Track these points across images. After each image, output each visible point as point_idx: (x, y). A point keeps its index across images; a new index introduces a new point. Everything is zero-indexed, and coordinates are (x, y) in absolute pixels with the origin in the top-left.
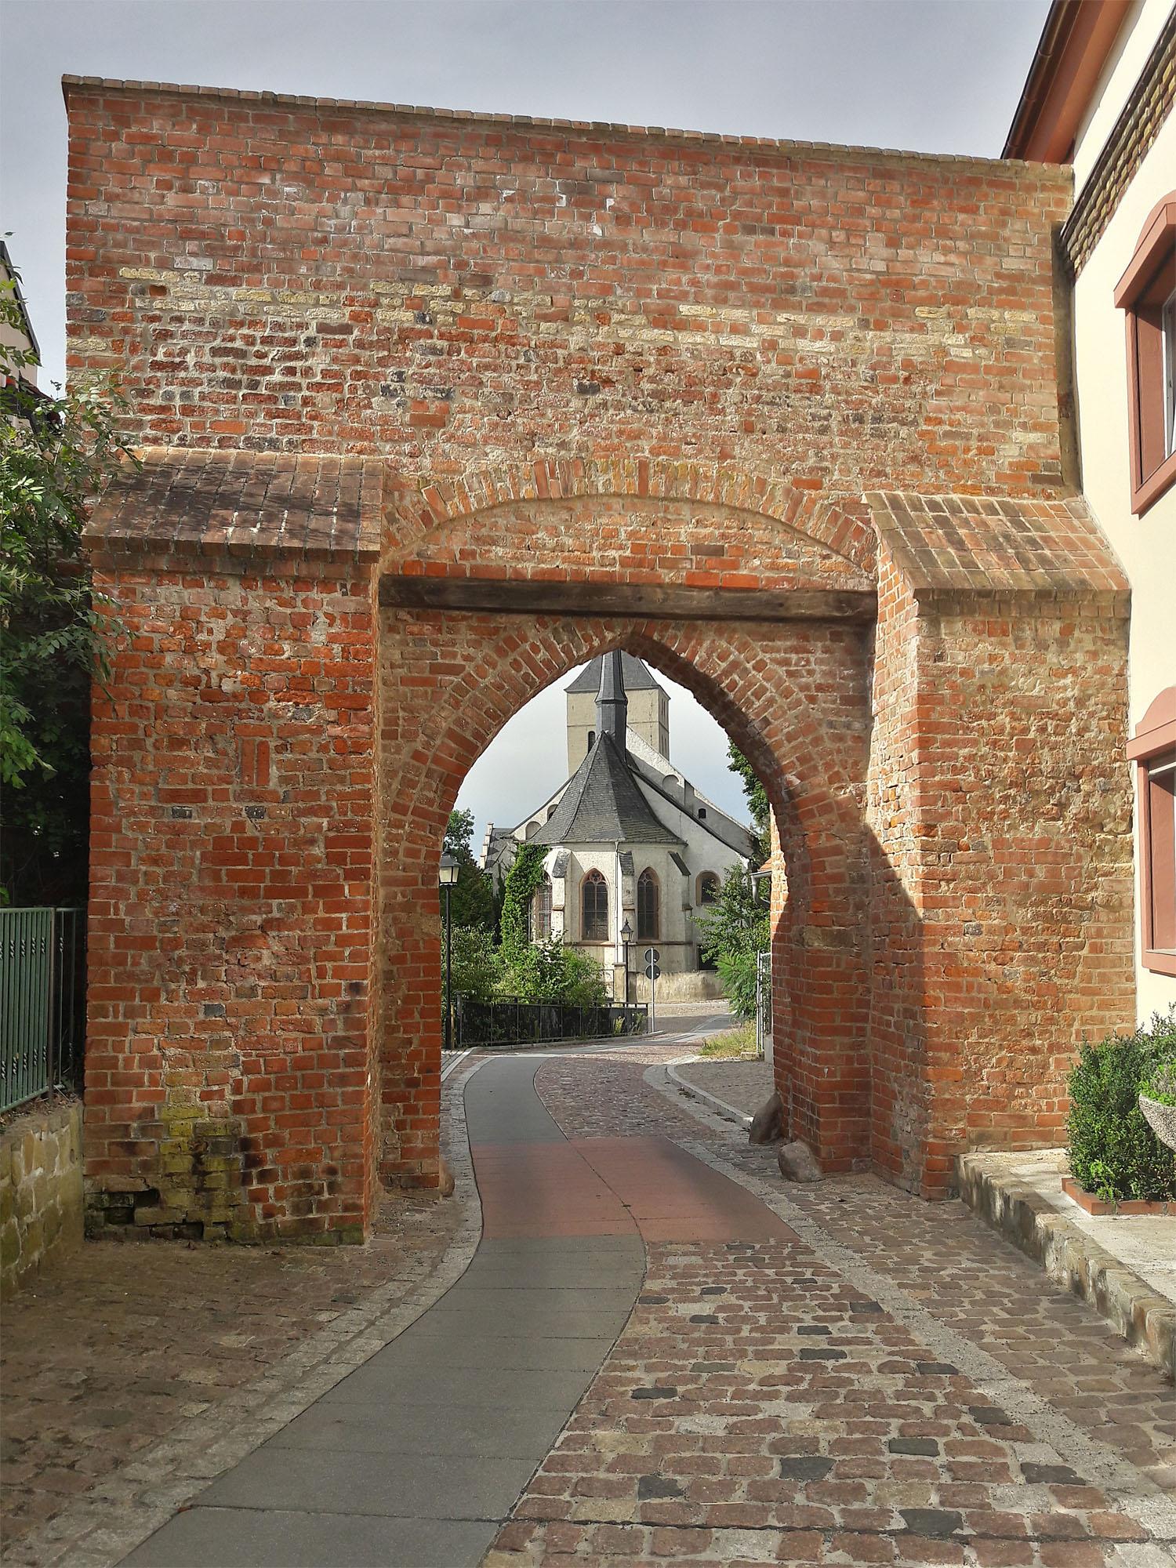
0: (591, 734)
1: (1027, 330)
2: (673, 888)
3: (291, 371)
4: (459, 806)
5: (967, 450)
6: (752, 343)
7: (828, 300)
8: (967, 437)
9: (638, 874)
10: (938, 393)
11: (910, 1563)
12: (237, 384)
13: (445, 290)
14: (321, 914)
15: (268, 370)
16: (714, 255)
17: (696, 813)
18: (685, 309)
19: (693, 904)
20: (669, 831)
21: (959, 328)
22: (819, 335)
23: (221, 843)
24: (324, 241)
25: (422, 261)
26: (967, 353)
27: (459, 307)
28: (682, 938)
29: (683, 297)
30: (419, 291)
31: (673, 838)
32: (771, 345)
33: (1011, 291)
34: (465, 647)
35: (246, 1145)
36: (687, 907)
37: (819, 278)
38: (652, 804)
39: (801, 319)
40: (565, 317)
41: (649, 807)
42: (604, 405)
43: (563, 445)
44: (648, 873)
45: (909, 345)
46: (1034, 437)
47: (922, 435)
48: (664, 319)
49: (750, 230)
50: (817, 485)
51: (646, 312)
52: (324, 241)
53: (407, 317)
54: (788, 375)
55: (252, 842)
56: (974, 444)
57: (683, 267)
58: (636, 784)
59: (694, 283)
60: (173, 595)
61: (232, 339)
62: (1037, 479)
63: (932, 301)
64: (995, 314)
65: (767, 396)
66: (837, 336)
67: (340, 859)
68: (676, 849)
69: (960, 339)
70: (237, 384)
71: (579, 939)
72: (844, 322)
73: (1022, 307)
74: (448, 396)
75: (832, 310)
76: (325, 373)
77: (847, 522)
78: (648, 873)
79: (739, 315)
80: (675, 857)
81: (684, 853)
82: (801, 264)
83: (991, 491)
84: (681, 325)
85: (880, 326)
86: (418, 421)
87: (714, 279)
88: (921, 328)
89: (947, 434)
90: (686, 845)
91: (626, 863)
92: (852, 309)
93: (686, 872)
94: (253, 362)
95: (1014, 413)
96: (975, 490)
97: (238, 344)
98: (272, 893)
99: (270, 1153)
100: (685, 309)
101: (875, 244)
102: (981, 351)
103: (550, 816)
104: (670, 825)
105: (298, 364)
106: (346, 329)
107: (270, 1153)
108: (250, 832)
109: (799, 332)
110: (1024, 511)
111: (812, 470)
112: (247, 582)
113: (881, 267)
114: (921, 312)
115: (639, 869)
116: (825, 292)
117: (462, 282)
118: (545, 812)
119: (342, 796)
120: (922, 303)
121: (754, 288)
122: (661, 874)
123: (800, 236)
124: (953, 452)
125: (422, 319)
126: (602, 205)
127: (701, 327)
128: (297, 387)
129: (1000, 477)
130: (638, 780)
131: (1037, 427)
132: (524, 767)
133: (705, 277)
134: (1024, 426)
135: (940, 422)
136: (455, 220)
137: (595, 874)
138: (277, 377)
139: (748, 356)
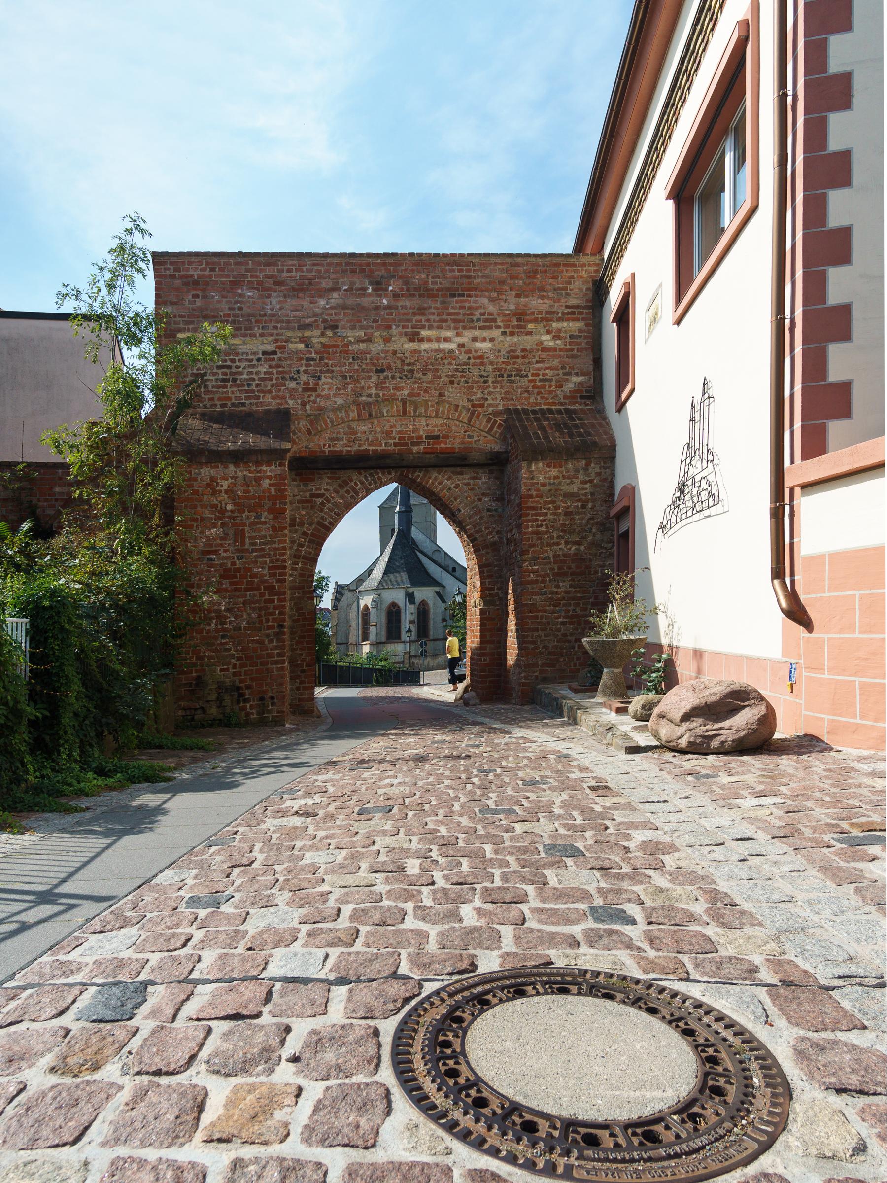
1: (580, 331)
3: (251, 373)
5: (550, 386)
6: (453, 346)
7: (489, 322)
8: (551, 380)
10: (537, 362)
12: (227, 380)
13: (317, 333)
14: (267, 597)
15: (241, 373)
16: (436, 308)
18: (424, 333)
21: (548, 332)
22: (484, 340)
23: (226, 570)
24: (265, 315)
25: (308, 321)
26: (551, 343)
27: (323, 340)
29: (423, 327)
30: (307, 333)
32: (461, 346)
33: (573, 313)
34: (324, 484)
35: (238, 688)
37: (483, 314)
39: (477, 333)
40: (369, 340)
42: (387, 377)
43: (369, 396)
45: (528, 342)
46: (580, 379)
47: (530, 381)
48: (414, 337)
49: (453, 296)
50: (482, 406)
51: (406, 334)
52: (265, 315)
53: (301, 346)
54: (469, 358)
55: (239, 570)
56: (554, 383)
57: (423, 314)
59: (428, 320)
60: (206, 472)
61: (226, 361)
62: (582, 397)
63: (535, 321)
64: (565, 324)
65: (461, 368)
66: (492, 340)
67: (274, 575)
68: (438, 589)
69: (548, 337)
70: (227, 380)
72: (496, 333)
73: (578, 320)
74: (319, 378)
75: (490, 328)
76: (265, 373)
77: (495, 422)
79: (449, 334)
80: (438, 593)
82: (477, 308)
83: (561, 404)
84: (421, 340)
85: (512, 334)
86: (305, 390)
87: (437, 319)
88: (530, 333)
89: (541, 380)
91: (411, 598)
92: (498, 327)
93: (444, 601)
94: (234, 370)
95: (572, 368)
96: (554, 404)
97: (228, 363)
98: (247, 590)
99: (247, 692)
100: (424, 333)
101: (511, 296)
102: (558, 342)
104: (436, 576)
105: (254, 370)
106: (275, 353)
107: (247, 692)
108: (238, 565)
109: (475, 339)
110: (575, 411)
111: (480, 399)
112: (236, 465)
113: (512, 307)
114: (530, 326)
116: (486, 321)
117: (325, 328)
119: (275, 549)
120: (531, 321)
121: (454, 321)
123: (476, 296)
124: (544, 387)
125: (307, 346)
126: (387, 290)
127: (429, 340)
128: (254, 380)
129: (565, 397)
131: (583, 374)
132: (353, 547)
133: (432, 317)
134: (577, 374)
135: (538, 375)
136: (322, 302)
137: (394, 605)
138: (245, 376)
139: (451, 351)
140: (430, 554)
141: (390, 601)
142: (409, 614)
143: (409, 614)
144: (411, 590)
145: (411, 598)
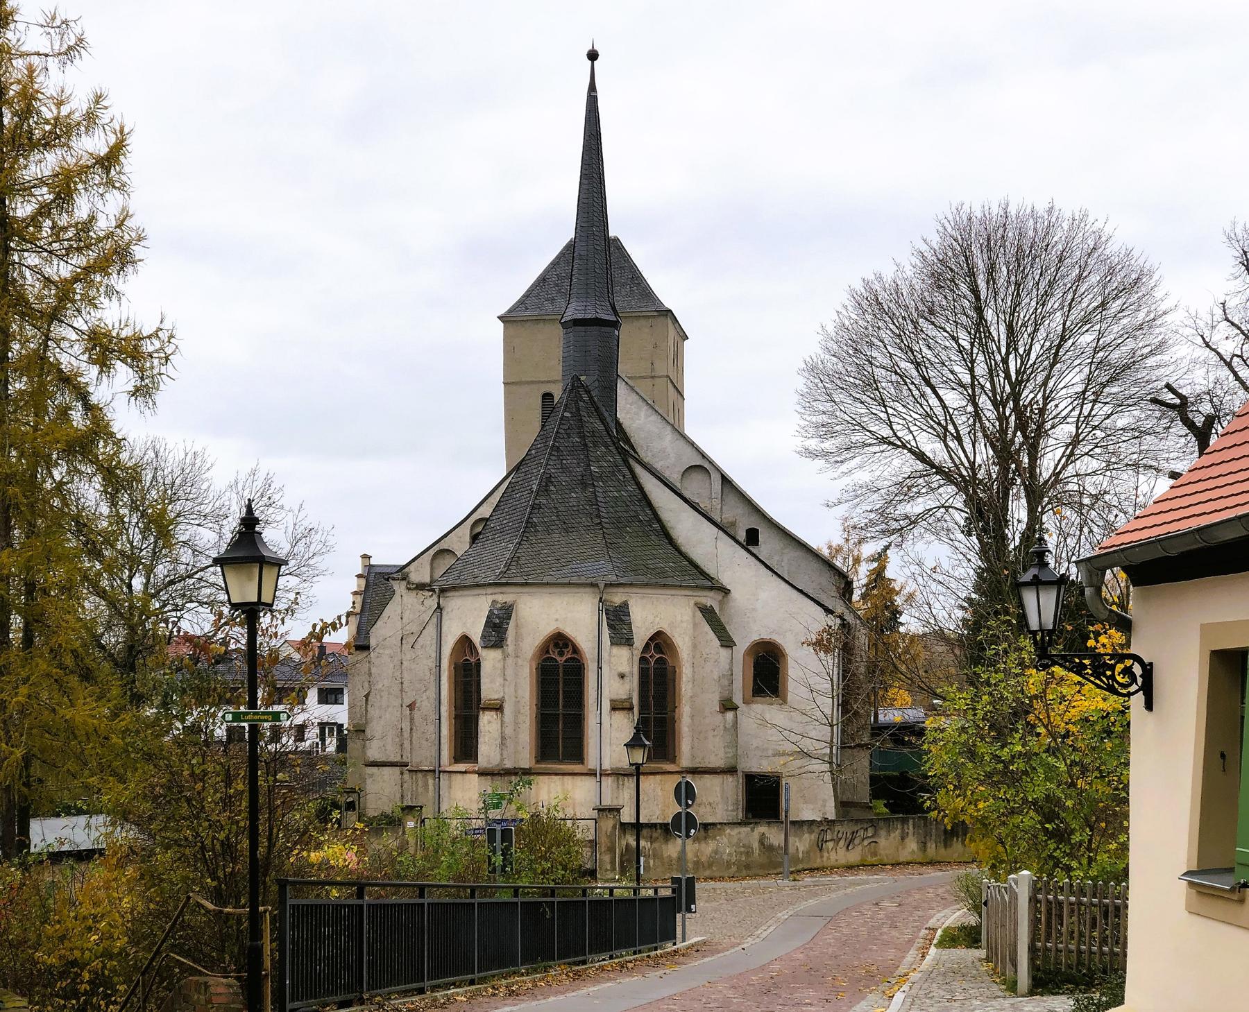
0: (547, 397)
2: (704, 671)
4: (611, 234)
9: (639, 643)
11: (314, 1004)
17: (742, 536)
19: (738, 699)
20: (696, 566)
28: (717, 761)
31: (696, 577)
36: (727, 706)
38: (665, 516)
41: (659, 520)
44: (659, 642)
58: (634, 477)
68: (710, 599)
71: (525, 757)
78: (659, 642)
80: (708, 614)
81: (722, 603)
90: (725, 591)
91: (617, 622)
93: (727, 642)
103: (474, 538)
115: (641, 634)
118: (465, 532)
122: (682, 643)
130: (638, 470)
137: (560, 641)
140: (674, 477)
141: (545, 629)
142: (612, 676)
143: (612, 676)
144: (617, 598)
145: (617, 622)
